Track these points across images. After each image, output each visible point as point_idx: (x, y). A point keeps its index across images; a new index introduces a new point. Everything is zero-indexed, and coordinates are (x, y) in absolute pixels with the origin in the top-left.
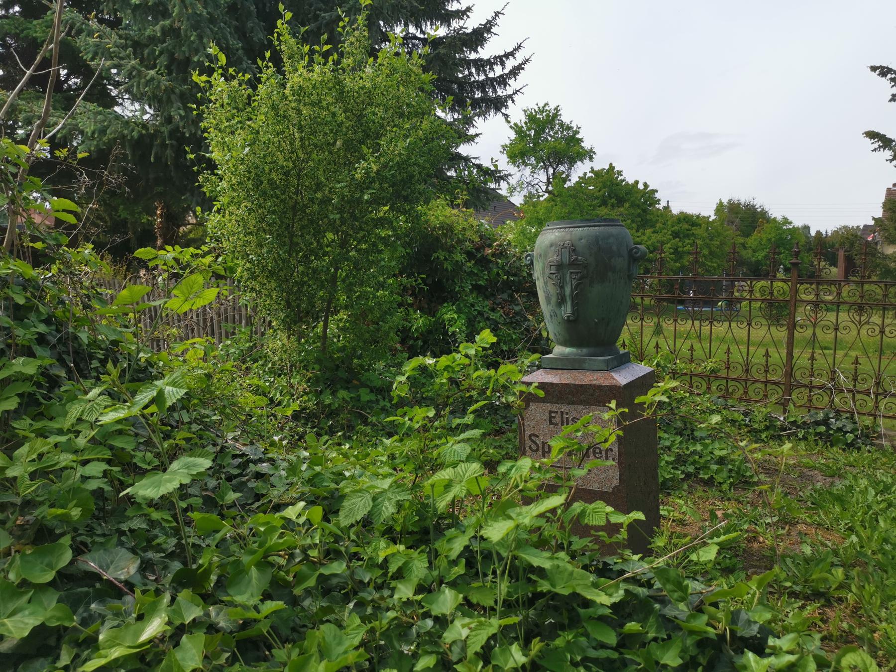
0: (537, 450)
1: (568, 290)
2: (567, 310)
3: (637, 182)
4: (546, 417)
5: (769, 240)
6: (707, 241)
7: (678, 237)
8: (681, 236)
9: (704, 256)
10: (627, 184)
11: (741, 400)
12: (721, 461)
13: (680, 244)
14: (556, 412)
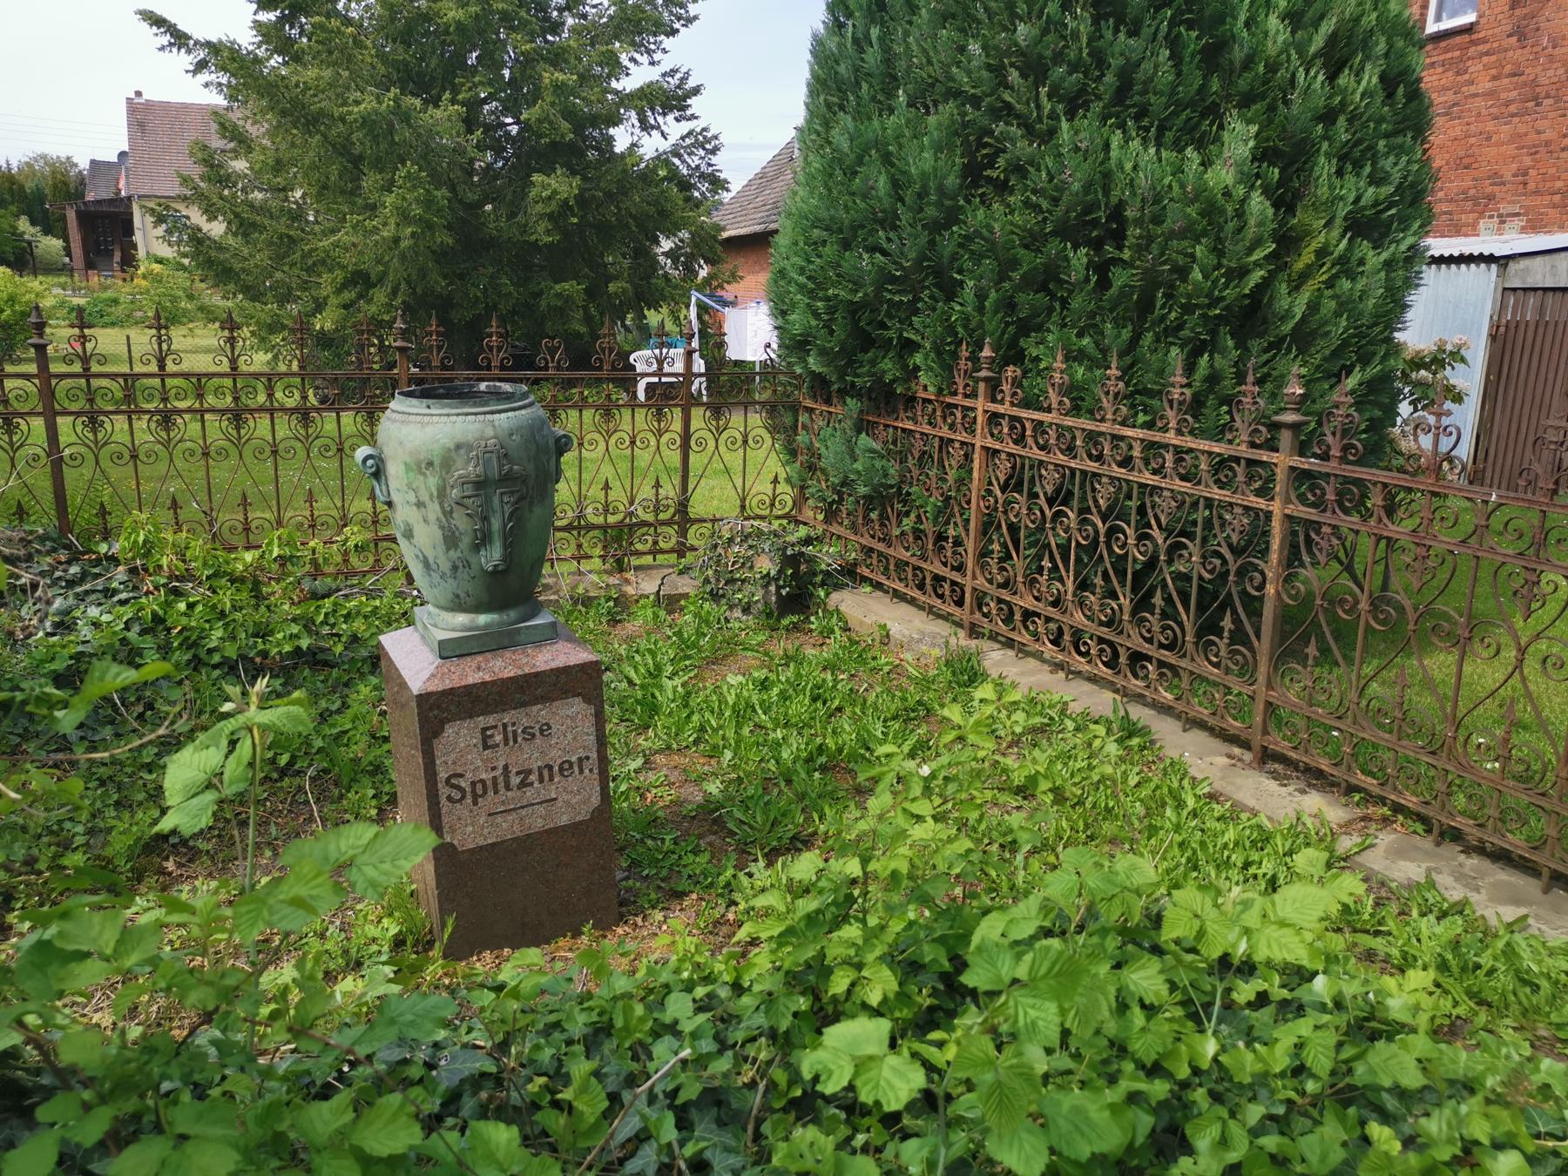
0: (463, 797)
1: (496, 524)
4: (476, 740)
14: (495, 727)
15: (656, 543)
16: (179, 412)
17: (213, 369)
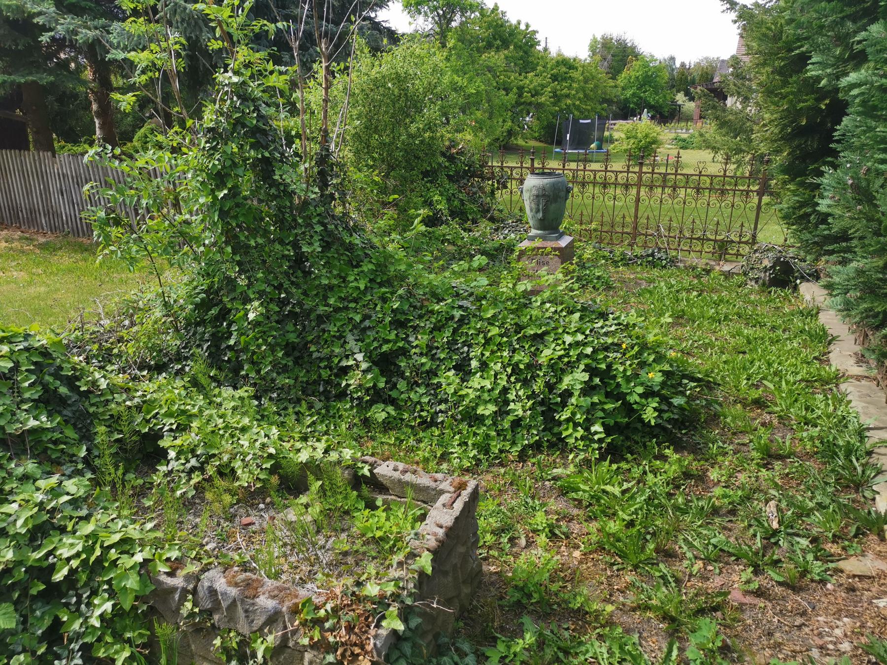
1: (541, 207)
2: (540, 215)
3: (519, 23)
5: (637, 78)
6: (582, 84)
7: (556, 80)
8: (560, 79)
9: (579, 99)
10: (511, 25)
11: (608, 244)
12: (599, 278)
13: (558, 87)
15: (738, 251)
16: (752, 191)
17: (694, 173)
